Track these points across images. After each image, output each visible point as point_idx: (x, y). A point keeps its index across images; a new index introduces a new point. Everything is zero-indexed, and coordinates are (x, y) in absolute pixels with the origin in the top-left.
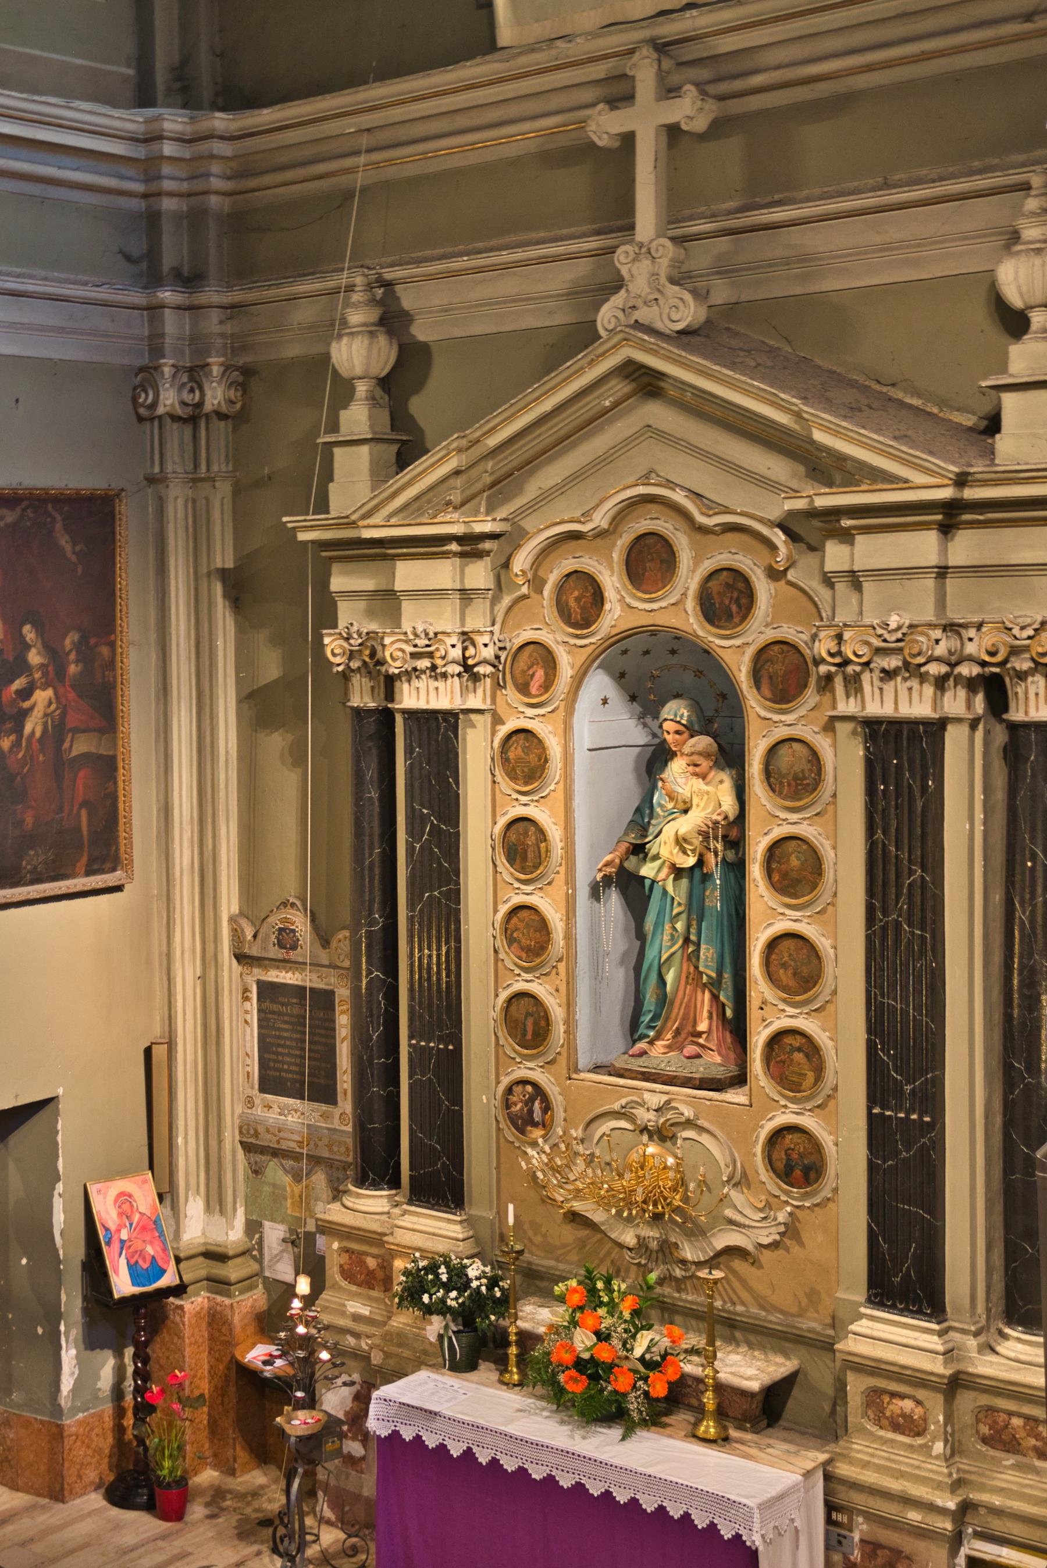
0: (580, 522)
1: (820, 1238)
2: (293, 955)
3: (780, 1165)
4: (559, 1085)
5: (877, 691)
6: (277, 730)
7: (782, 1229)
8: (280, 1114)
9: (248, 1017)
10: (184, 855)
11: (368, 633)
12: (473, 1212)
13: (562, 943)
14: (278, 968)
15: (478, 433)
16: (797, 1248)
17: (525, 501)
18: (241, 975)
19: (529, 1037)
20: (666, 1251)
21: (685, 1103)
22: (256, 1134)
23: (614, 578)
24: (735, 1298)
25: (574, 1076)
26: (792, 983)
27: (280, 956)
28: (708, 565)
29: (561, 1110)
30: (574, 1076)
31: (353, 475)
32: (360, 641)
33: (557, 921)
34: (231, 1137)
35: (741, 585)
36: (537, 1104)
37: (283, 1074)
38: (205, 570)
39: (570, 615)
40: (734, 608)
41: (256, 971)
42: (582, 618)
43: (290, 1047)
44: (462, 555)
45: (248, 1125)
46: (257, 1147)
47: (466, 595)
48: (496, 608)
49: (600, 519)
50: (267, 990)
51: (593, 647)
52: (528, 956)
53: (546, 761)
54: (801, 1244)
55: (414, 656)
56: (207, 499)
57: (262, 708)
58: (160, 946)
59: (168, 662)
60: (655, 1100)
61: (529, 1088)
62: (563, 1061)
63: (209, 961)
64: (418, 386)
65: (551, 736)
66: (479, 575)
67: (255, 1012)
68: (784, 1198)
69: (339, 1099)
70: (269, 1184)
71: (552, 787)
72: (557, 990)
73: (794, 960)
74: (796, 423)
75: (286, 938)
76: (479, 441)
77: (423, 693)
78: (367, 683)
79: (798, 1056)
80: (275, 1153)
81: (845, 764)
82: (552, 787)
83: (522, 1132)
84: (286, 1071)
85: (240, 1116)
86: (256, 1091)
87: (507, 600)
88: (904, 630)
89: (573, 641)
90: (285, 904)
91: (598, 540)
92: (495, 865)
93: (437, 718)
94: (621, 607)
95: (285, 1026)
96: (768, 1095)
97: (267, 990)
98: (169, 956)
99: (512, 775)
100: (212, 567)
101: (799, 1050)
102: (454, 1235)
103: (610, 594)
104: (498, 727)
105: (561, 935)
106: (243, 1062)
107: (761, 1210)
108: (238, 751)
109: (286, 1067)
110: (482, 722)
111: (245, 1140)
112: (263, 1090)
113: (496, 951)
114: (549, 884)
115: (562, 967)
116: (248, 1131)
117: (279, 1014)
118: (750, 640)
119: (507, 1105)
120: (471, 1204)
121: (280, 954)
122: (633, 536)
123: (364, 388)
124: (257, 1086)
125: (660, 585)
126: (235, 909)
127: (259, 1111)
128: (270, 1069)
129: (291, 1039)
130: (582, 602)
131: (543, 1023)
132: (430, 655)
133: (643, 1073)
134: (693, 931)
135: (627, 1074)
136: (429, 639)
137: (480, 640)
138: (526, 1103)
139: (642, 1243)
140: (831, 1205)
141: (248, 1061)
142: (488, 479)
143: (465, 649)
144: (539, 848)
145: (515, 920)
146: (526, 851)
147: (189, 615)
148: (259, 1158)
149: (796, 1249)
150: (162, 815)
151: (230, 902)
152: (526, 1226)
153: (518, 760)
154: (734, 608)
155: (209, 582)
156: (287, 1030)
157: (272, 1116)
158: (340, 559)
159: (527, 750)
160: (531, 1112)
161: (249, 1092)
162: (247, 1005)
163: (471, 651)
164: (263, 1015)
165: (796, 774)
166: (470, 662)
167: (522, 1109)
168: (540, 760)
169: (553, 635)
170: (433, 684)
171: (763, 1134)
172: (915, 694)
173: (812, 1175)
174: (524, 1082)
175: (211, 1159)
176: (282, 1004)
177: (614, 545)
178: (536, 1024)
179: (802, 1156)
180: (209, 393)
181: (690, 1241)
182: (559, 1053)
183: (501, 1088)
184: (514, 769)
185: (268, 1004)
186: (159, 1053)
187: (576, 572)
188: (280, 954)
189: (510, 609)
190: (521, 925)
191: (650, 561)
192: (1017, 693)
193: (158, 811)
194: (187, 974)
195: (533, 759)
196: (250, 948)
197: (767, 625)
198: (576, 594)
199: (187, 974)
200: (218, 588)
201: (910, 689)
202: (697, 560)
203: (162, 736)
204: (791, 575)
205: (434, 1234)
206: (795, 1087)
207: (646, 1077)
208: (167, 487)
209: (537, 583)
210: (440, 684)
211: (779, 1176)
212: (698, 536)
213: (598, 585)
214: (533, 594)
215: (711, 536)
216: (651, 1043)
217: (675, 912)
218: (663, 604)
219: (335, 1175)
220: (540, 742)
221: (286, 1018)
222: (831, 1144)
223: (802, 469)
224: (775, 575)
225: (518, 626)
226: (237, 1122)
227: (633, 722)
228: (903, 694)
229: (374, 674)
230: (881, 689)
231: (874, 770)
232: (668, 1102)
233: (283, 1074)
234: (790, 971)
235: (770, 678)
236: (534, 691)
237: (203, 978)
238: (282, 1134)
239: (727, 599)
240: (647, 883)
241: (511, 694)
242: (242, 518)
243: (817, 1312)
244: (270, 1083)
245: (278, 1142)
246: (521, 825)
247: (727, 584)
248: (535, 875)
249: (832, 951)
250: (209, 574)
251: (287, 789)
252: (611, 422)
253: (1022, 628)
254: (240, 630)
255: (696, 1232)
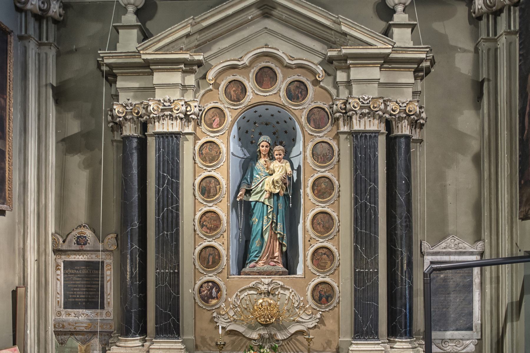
0: (238, 61)
1: (331, 321)
2: (84, 248)
3: (317, 298)
4: (223, 281)
5: (358, 122)
6: (77, 154)
7: (318, 320)
8: (75, 317)
9: (59, 277)
10: (32, 206)
11: (135, 105)
12: (184, 338)
13: (226, 225)
14: (75, 254)
15: (200, 19)
16: (323, 326)
17: (212, 53)
18: (55, 259)
19: (210, 263)
20: (272, 337)
21: (279, 280)
22: (63, 326)
23: (250, 84)
24: (298, 350)
25: (230, 277)
26: (322, 230)
27: (78, 248)
28: (289, 80)
29: (225, 291)
30: (230, 277)
31: (129, 41)
32: (131, 108)
33: (224, 216)
34: (51, 329)
35: (303, 87)
36: (214, 290)
37: (77, 300)
38: (44, 84)
39: (231, 97)
40: (300, 95)
41: (63, 257)
42: (237, 98)
43: (81, 288)
44: (184, 72)
45: (59, 323)
46: (62, 332)
47: (185, 88)
48: (197, 95)
49: (246, 60)
50: (68, 265)
51: (241, 109)
52: (210, 231)
53: (220, 153)
54: (325, 325)
55: (162, 110)
56: (46, 54)
57: (68, 145)
58: (19, 244)
59: (27, 118)
60: (267, 281)
61: (210, 284)
62: (225, 271)
63: (40, 252)
64: (151, 18)
65: (222, 144)
66: (191, 80)
67: (62, 275)
68: (318, 309)
69: (105, 306)
70: (69, 348)
71: (222, 164)
72: (223, 244)
73: (323, 221)
74: (333, 25)
75: (81, 240)
76: (199, 23)
77: (165, 126)
78: (133, 126)
79: (325, 257)
80: (72, 333)
81: (344, 149)
82: (222, 164)
83: (207, 302)
84: (78, 298)
85: (54, 320)
86: (62, 309)
87: (202, 92)
88: (370, 99)
89: (232, 107)
90: (80, 226)
91: (243, 70)
92: (195, 196)
93: (172, 137)
94: (253, 94)
95: (78, 279)
96: (312, 273)
97: (68, 265)
98: (24, 249)
99: (204, 159)
100: (48, 82)
101: (325, 254)
102: (180, 347)
103: (249, 90)
104: (197, 141)
105: (225, 222)
106: (56, 297)
107: (309, 315)
108: (56, 162)
109: (78, 296)
110: (191, 138)
111: (57, 330)
112: (65, 308)
113: (195, 231)
114: (220, 202)
115: (225, 234)
116: (59, 326)
117: (75, 274)
118: (306, 107)
119: (200, 292)
120: (183, 335)
121: (78, 247)
122: (259, 68)
123: (132, 10)
124: (63, 307)
125: (270, 86)
126: (53, 231)
127: (64, 317)
128: (69, 298)
129: (81, 284)
130: (237, 91)
131: (217, 257)
132: (171, 110)
133: (258, 272)
134: (275, 218)
135: (252, 273)
136: (171, 103)
137: (193, 104)
138: (209, 290)
139: (261, 337)
140: (336, 309)
141: (58, 296)
142: (197, 43)
143: (186, 108)
144: (216, 188)
145: (204, 217)
146: (210, 190)
147: (35, 102)
148: (63, 337)
149: (322, 327)
150: (22, 186)
151: (51, 228)
152: (208, 340)
153: (206, 154)
154: (300, 95)
155: (46, 88)
156: (79, 281)
157: (71, 318)
158: (122, 74)
159: (211, 150)
160: (211, 293)
161: (58, 309)
162: (58, 272)
163: (189, 109)
164: (66, 275)
165: (323, 154)
166: (188, 113)
167: (207, 293)
168: (217, 153)
169: (224, 104)
170: (170, 122)
171: (311, 287)
172: (372, 123)
173: (329, 298)
174: (208, 282)
175: (41, 340)
176: (77, 270)
177: (250, 71)
178: (213, 258)
179: (325, 292)
180: (52, 6)
181: (280, 333)
182: (224, 269)
183: (197, 286)
184: (205, 157)
185: (70, 271)
186: (21, 291)
187: (234, 80)
188: (78, 247)
189: (203, 95)
190: (207, 219)
191: (266, 77)
192: (398, 126)
193: (20, 185)
194: (31, 257)
195: (214, 153)
196: (61, 247)
197: (312, 102)
198: (234, 89)
199: (31, 257)
200: (50, 92)
201: (370, 121)
202: (284, 78)
203: (23, 151)
204: (321, 84)
205: (170, 349)
206: (323, 268)
207: (260, 273)
208: (29, 42)
209: (216, 86)
210: (174, 122)
211: (316, 302)
212: (285, 69)
213: (244, 85)
214: (214, 90)
215: (290, 69)
216: (257, 263)
217: (269, 211)
218: (271, 93)
219: (103, 338)
220: (217, 145)
221: (78, 276)
222: (336, 286)
223: (326, 47)
224: (316, 83)
225: (207, 102)
226: (53, 322)
227: (240, 148)
228: (368, 123)
229: (136, 122)
230: (360, 121)
231: (356, 151)
232: (272, 281)
233: (77, 300)
234: (321, 226)
235: (314, 120)
236: (214, 126)
237: (38, 261)
238: (77, 325)
239: (297, 92)
240: (253, 204)
241: (204, 127)
242: (60, 65)
243: (330, 348)
244: (70, 303)
245: (75, 328)
246: (208, 179)
247: (297, 86)
248: (214, 198)
249: (337, 218)
250: (46, 85)
251: (80, 179)
252: (249, 26)
253: (403, 103)
254: (58, 112)
255: (282, 328)
